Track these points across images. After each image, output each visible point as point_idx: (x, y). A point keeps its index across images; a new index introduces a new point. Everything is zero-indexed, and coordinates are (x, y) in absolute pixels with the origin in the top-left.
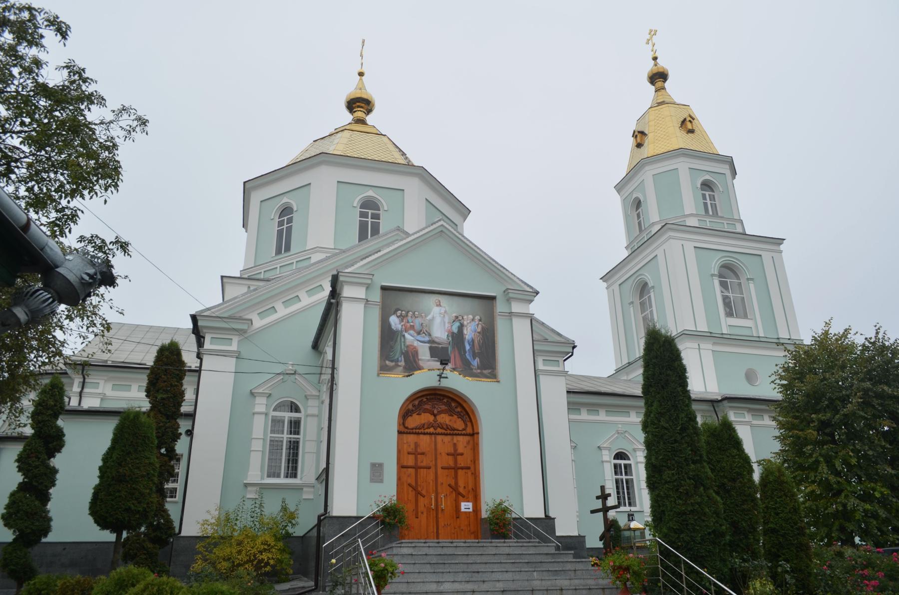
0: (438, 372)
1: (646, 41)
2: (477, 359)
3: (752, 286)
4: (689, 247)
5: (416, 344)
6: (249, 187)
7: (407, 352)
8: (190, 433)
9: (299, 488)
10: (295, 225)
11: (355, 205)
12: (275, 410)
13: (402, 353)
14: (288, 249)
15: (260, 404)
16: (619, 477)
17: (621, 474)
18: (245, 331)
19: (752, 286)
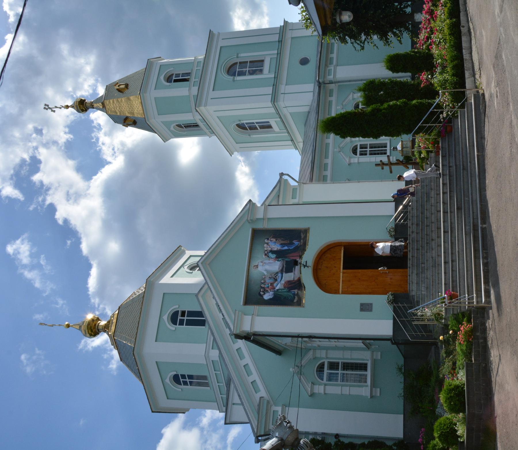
0: (302, 267)
1: (53, 112)
2: (294, 242)
3: (242, 55)
4: (212, 94)
5: (283, 282)
6: (153, 412)
7: (288, 288)
9: (374, 362)
10: (186, 373)
11: (174, 329)
12: (322, 379)
13: (289, 291)
14: (205, 378)
15: (319, 389)
16: (368, 152)
17: (367, 151)
18: (268, 402)
19: (242, 55)
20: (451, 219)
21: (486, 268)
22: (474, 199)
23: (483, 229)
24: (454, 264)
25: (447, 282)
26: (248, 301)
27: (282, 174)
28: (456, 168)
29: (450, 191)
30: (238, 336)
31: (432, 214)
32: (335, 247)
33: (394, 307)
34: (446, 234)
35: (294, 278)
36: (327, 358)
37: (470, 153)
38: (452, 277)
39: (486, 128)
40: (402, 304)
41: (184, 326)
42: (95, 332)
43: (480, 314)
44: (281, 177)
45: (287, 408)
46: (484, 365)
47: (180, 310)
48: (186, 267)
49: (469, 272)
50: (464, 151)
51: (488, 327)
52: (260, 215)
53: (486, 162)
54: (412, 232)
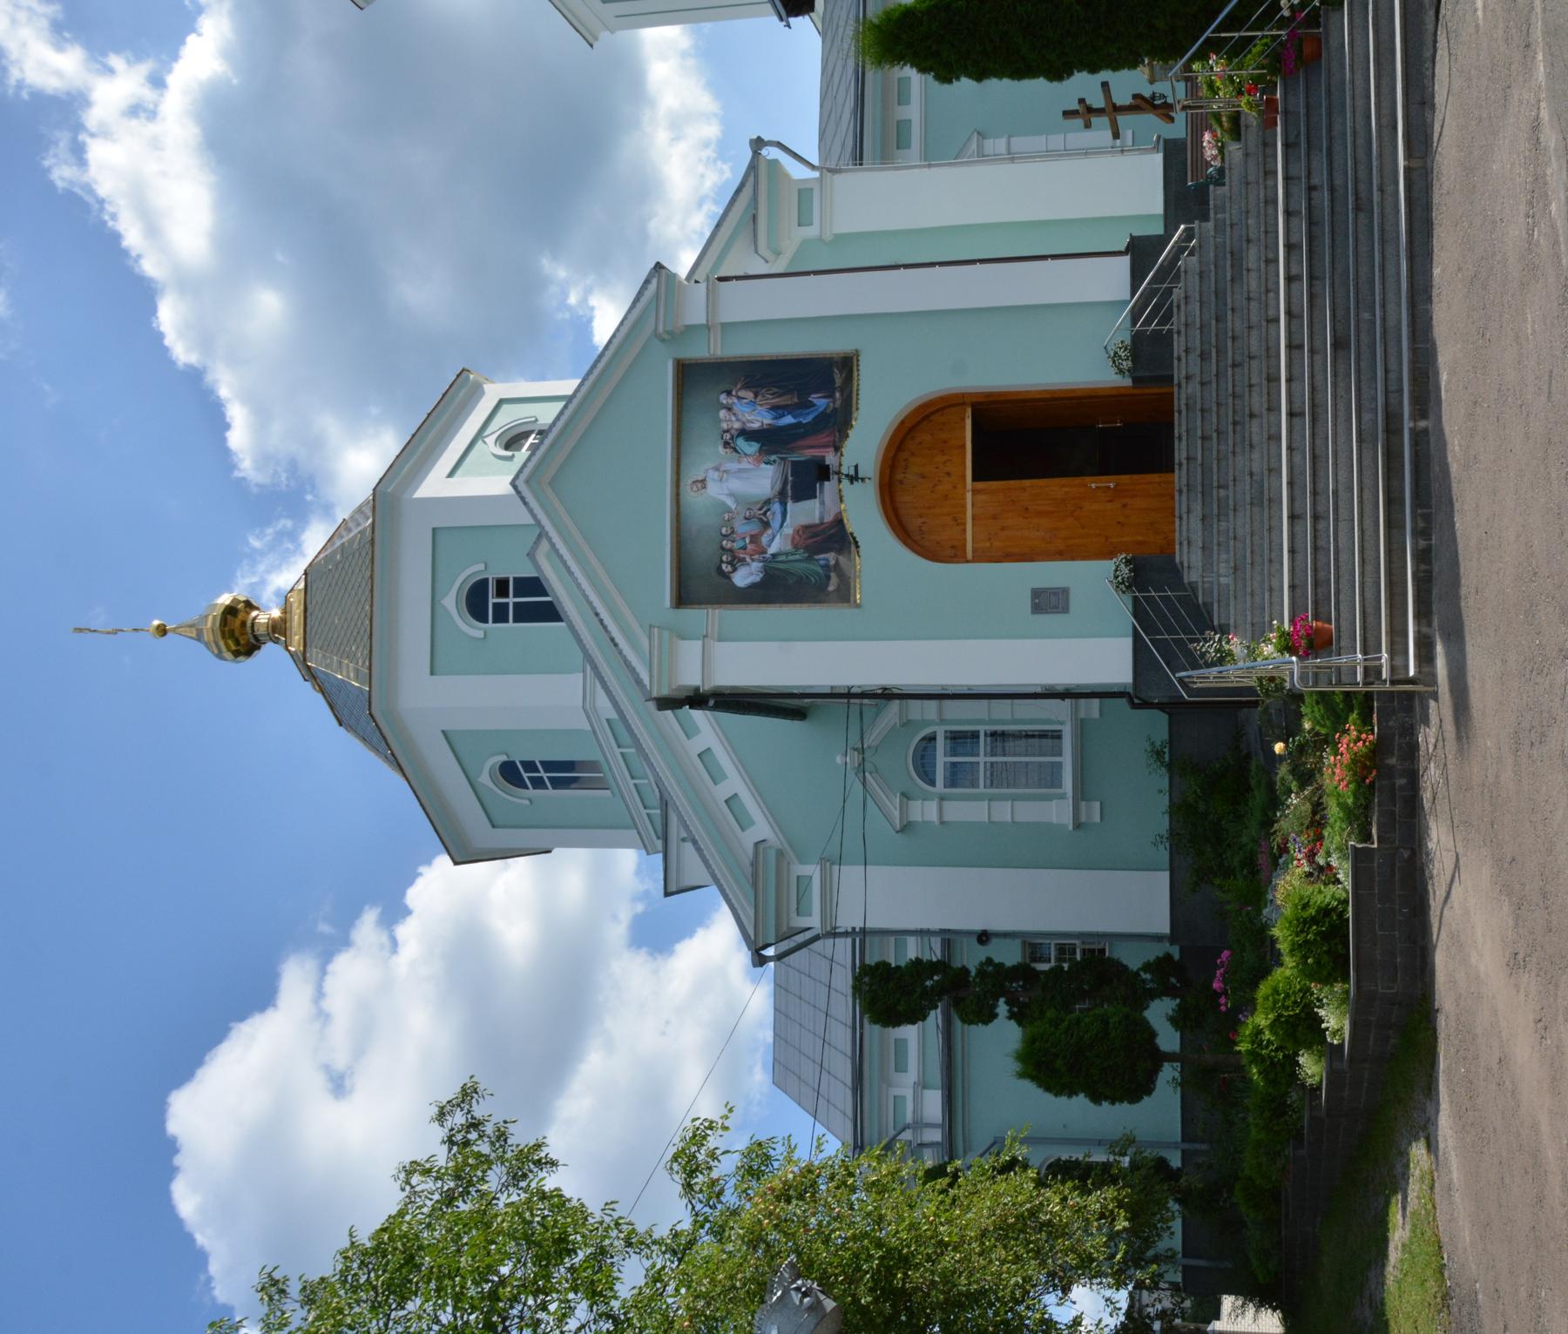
0: (845, 482)
2: (814, 398)
5: (788, 530)
7: (807, 548)
8: (984, 937)
11: (480, 634)
12: (932, 783)
13: (810, 559)
14: (592, 766)
15: (925, 811)
18: (780, 854)
20: (1312, 377)
21: (1423, 567)
22: (1391, 322)
23: (1419, 438)
24: (1321, 526)
25: (1297, 582)
26: (683, 597)
27: (758, 144)
28: (1332, 200)
29: (1311, 277)
30: (666, 703)
31: (1249, 241)
32: (943, 409)
33: (1135, 599)
34: (1296, 420)
35: (822, 518)
36: (942, 721)
37: (1380, 155)
38: (1315, 570)
39: (1441, 69)
40: (1168, 612)
41: (511, 624)
42: (248, 643)
43: (1392, 716)
44: (756, 153)
45: (836, 868)
46: (1406, 854)
47: (492, 575)
48: (491, 440)
49: (1369, 568)
50: (1360, 141)
51: (1423, 748)
52: (695, 313)
53: (1436, 199)
54: (1188, 378)
